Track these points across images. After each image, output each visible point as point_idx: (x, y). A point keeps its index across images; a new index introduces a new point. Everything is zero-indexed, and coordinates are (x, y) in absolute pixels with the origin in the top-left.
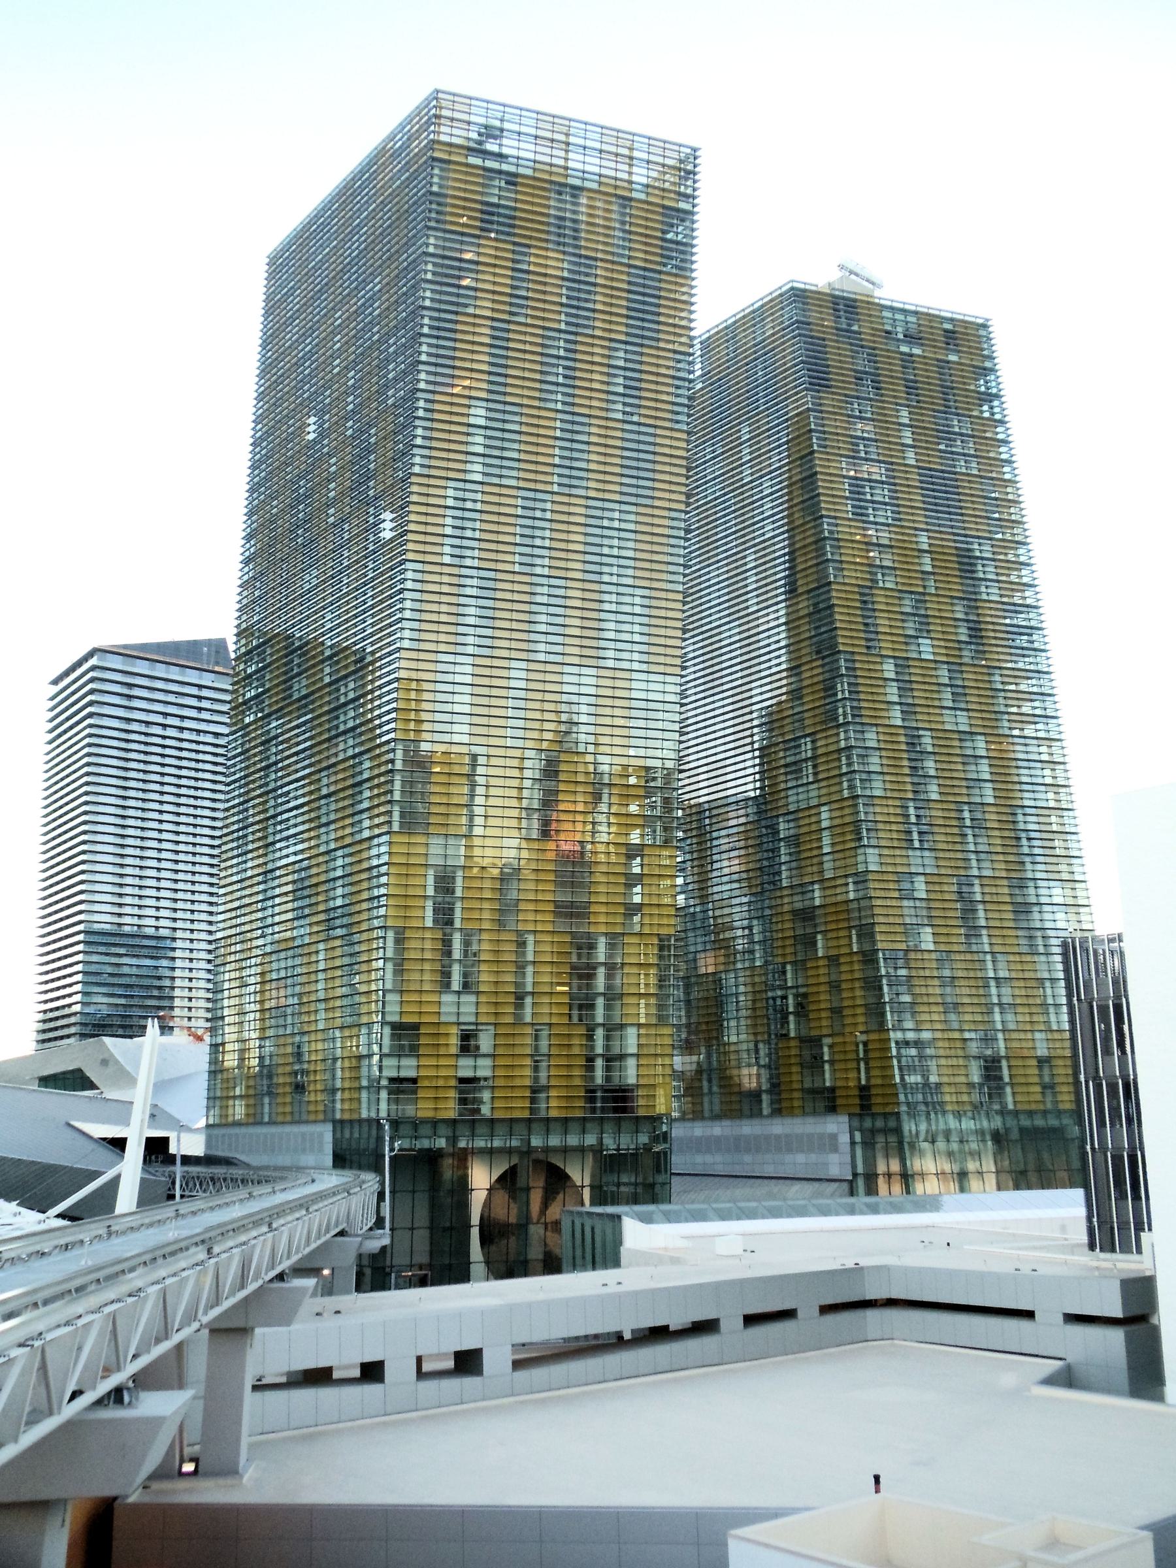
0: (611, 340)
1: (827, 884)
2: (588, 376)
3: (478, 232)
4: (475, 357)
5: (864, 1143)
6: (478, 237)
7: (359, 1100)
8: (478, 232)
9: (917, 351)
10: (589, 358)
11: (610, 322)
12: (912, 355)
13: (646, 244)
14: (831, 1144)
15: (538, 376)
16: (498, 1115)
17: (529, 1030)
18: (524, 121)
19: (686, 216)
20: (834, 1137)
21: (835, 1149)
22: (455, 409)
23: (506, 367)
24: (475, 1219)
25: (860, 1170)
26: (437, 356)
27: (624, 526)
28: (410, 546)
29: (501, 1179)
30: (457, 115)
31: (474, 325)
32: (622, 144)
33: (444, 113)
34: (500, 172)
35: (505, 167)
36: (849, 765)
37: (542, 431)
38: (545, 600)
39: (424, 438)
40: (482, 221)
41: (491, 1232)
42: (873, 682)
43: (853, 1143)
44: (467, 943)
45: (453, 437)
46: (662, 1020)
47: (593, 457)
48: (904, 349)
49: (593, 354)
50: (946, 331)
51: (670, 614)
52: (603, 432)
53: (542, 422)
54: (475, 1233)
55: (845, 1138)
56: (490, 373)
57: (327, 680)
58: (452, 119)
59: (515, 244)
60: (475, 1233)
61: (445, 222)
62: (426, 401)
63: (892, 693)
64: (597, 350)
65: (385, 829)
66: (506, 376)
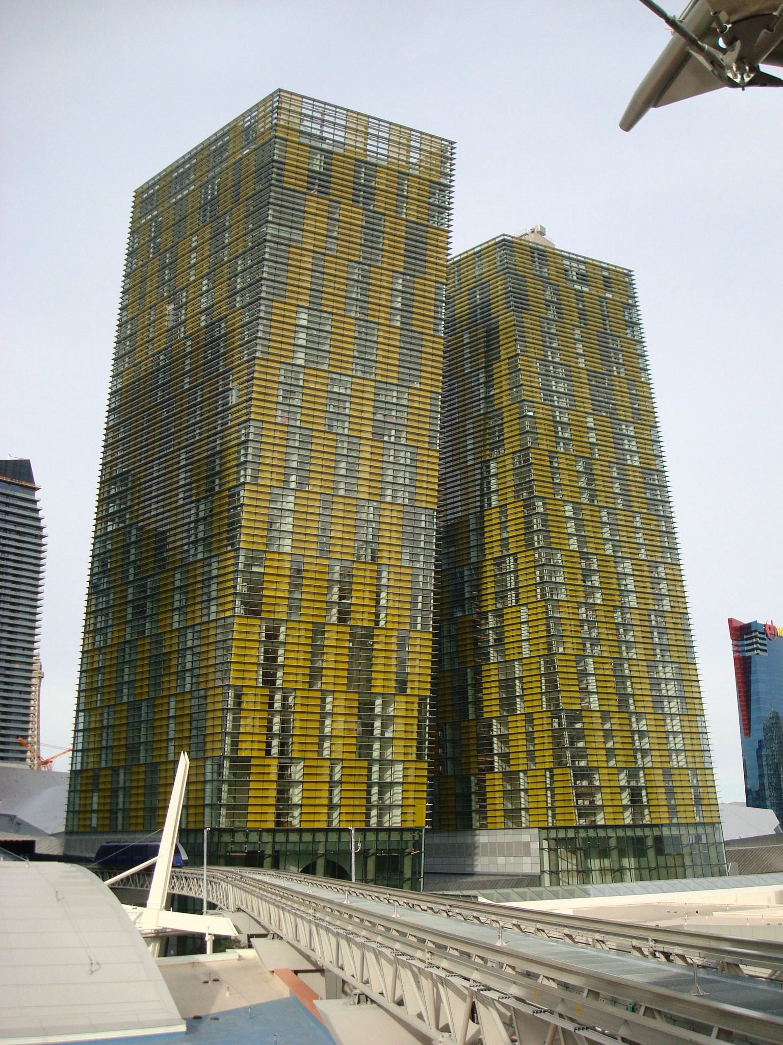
0: (394, 271)
1: (524, 662)
2: (376, 314)
3: (305, 190)
4: (300, 296)
5: (550, 849)
6: (305, 194)
7: (204, 790)
8: (305, 190)
9: (586, 289)
10: (378, 283)
11: (393, 259)
12: (582, 292)
13: (419, 183)
14: (525, 849)
15: (343, 294)
16: (305, 826)
17: (328, 763)
18: (338, 115)
19: (445, 188)
20: (527, 845)
21: (528, 854)
22: (286, 313)
23: (323, 286)
25: (546, 868)
26: (277, 256)
27: (399, 421)
28: (255, 389)
30: (292, 108)
31: (298, 293)
32: (402, 135)
33: (284, 105)
34: (322, 150)
35: (325, 146)
36: (541, 578)
37: (345, 333)
38: (340, 514)
39: (266, 312)
40: (308, 182)
42: (559, 519)
43: (541, 849)
44: (285, 698)
45: (283, 353)
46: (419, 757)
47: (382, 315)
48: (577, 287)
49: (380, 299)
50: (604, 277)
51: (431, 466)
52: (385, 373)
53: (345, 345)
55: (535, 846)
56: (311, 290)
57: (187, 387)
58: (290, 111)
59: (330, 200)
61: (284, 182)
62: (266, 306)
63: (571, 527)
64: (383, 296)
65: (231, 591)
66: (322, 292)
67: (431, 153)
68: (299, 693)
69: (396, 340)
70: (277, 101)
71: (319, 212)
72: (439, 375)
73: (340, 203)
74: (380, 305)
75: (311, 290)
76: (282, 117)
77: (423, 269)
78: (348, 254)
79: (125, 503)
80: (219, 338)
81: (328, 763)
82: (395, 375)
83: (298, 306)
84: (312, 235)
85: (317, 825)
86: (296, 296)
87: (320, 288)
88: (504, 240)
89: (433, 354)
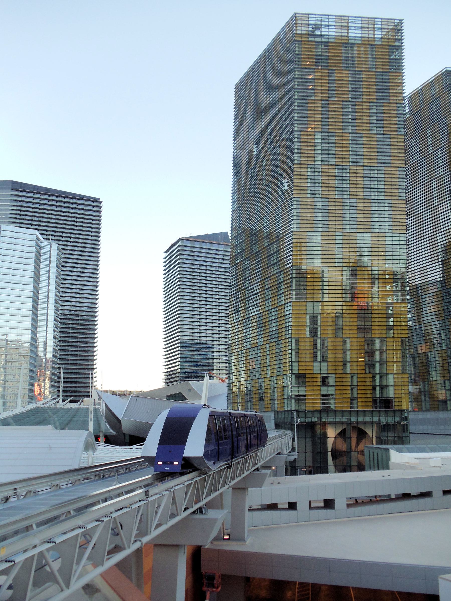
6: (315, 69)
17: (349, 376)
19: (399, 48)
24: (330, 449)
29: (340, 434)
31: (315, 103)
32: (369, 23)
33: (299, 22)
35: (323, 40)
39: (298, 149)
40: (315, 62)
41: (336, 454)
44: (323, 343)
52: (369, 161)
54: (330, 454)
60: (330, 454)
62: (298, 146)
67: (389, 39)
68: (330, 340)
69: (374, 99)
70: (294, 21)
71: (323, 78)
72: (402, 125)
73: (335, 70)
74: (363, 112)
75: (322, 100)
76: (298, 28)
77: (388, 81)
78: (342, 98)
79: (242, 248)
80: (273, 254)
81: (349, 376)
82: (375, 97)
83: (315, 132)
84: (321, 91)
85: (344, 409)
86: (314, 105)
87: (327, 127)
88: (446, 71)
89: (398, 146)
